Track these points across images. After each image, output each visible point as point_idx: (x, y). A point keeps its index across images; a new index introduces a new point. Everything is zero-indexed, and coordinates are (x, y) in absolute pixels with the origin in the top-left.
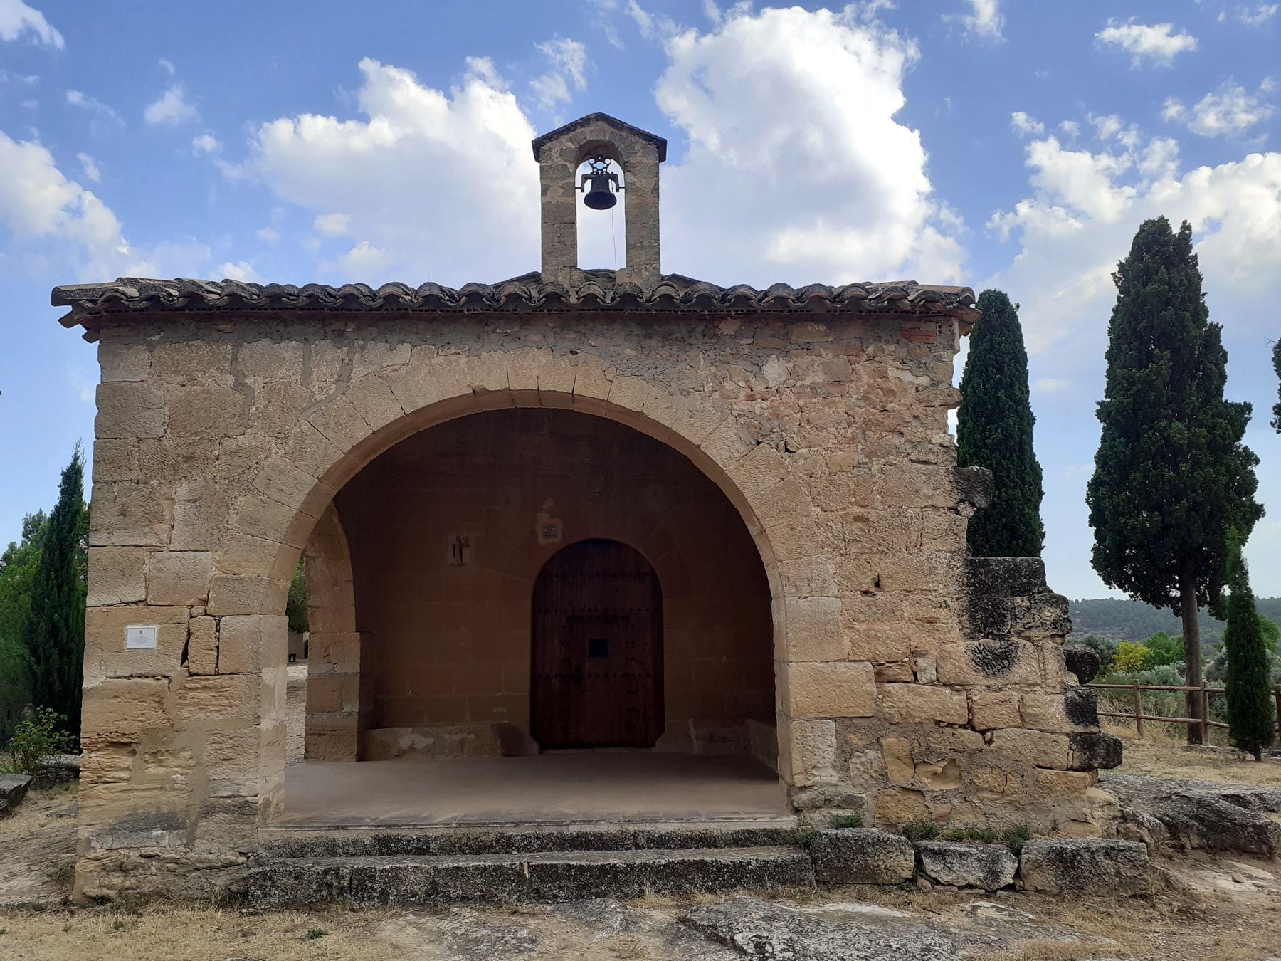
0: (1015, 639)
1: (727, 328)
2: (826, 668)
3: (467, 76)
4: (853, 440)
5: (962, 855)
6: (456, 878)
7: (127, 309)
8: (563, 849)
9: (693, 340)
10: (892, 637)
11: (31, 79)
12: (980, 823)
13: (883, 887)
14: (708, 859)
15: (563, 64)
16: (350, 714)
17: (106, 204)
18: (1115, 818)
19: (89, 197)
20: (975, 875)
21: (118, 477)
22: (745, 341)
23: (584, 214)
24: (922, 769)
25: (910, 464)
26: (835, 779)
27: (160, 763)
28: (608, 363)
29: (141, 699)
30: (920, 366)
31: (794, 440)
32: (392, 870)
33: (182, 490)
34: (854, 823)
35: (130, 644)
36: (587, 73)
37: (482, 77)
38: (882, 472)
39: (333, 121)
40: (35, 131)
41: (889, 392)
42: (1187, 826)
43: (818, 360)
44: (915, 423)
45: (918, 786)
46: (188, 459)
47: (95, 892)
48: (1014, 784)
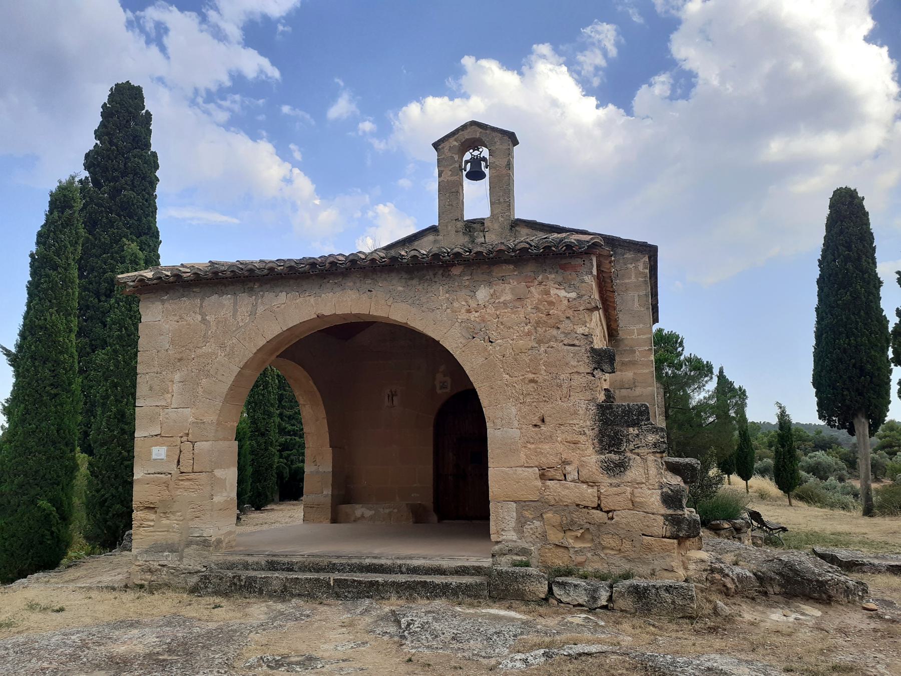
0: (629, 454)
1: (456, 271)
2: (510, 471)
3: (533, 57)
4: (529, 334)
5: (575, 586)
6: (296, 584)
7: (147, 285)
8: (362, 572)
9: (436, 279)
10: (551, 452)
11: (261, 102)
12: (603, 568)
13: (527, 602)
14: (428, 580)
15: (599, 41)
16: (326, 496)
17: (306, 175)
18: (705, 570)
19: (296, 171)
20: (583, 599)
21: (148, 371)
22: (466, 278)
23: (467, 184)
24: (569, 533)
25: (564, 347)
26: (515, 538)
27: (168, 518)
28: (388, 296)
29: (158, 485)
30: (571, 287)
31: (494, 335)
32: (265, 578)
33: (177, 377)
34: (527, 565)
35: (154, 457)
36: (617, 44)
37: (544, 57)
38: (546, 352)
39: (446, 99)
40: (264, 133)
41: (551, 303)
42: (771, 579)
43: (508, 287)
44: (567, 321)
45: (566, 544)
46: (180, 360)
47: (139, 582)
48: (627, 545)
